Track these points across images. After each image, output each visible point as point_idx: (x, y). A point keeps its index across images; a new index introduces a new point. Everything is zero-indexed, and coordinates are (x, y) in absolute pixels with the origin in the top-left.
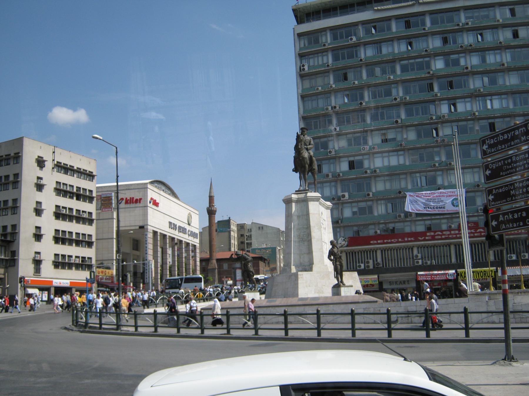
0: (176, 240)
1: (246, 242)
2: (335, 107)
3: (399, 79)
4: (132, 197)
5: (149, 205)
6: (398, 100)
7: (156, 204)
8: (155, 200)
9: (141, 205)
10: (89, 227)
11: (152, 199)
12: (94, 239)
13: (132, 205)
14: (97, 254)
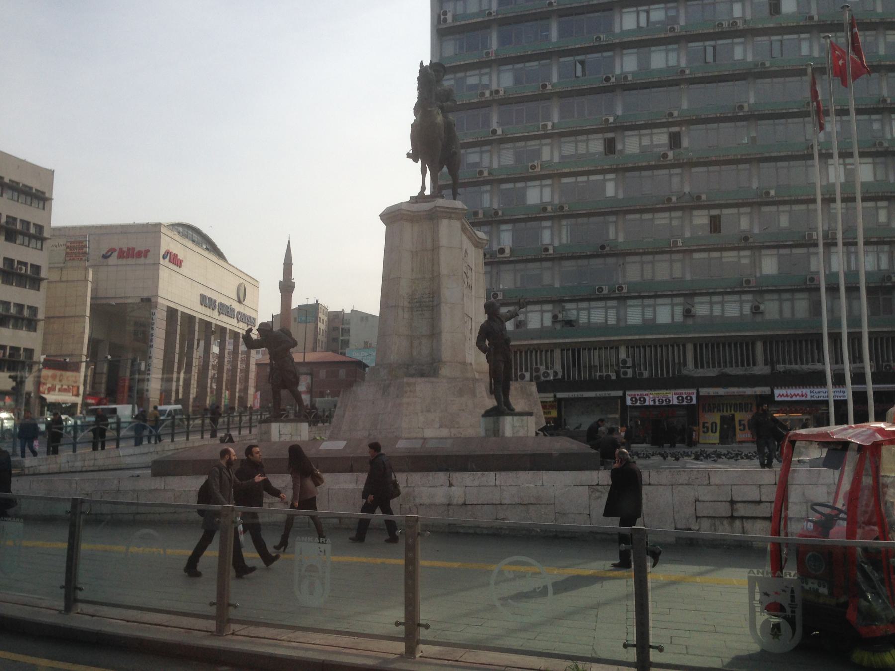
0: (213, 326)
1: (341, 338)
2: (497, 92)
3: (617, 41)
4: (131, 246)
5: (161, 261)
6: (613, 80)
7: (175, 261)
8: (175, 256)
9: (148, 261)
10: (32, 292)
11: (168, 253)
12: (41, 315)
13: (130, 261)
14: (45, 344)
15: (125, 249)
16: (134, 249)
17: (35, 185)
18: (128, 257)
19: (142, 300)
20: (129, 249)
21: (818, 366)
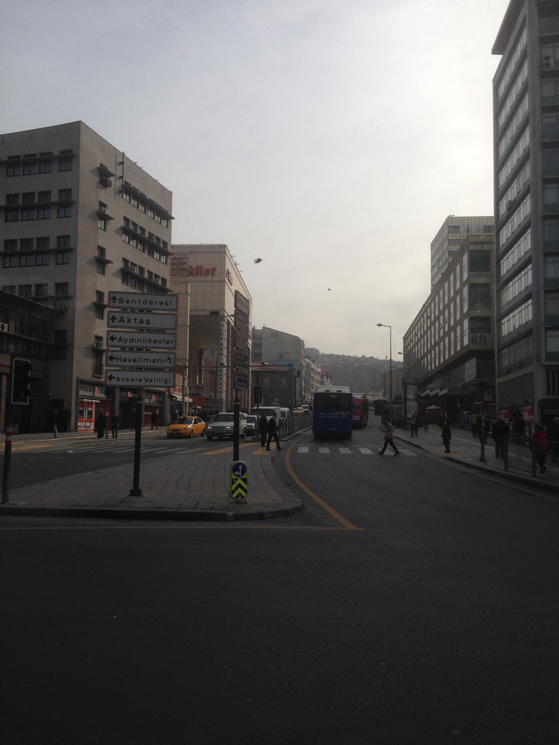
4: (199, 264)
13: (199, 278)
16: (202, 267)
17: (159, 201)
18: (196, 275)
19: (211, 312)
20: (197, 267)
21: (224, 410)
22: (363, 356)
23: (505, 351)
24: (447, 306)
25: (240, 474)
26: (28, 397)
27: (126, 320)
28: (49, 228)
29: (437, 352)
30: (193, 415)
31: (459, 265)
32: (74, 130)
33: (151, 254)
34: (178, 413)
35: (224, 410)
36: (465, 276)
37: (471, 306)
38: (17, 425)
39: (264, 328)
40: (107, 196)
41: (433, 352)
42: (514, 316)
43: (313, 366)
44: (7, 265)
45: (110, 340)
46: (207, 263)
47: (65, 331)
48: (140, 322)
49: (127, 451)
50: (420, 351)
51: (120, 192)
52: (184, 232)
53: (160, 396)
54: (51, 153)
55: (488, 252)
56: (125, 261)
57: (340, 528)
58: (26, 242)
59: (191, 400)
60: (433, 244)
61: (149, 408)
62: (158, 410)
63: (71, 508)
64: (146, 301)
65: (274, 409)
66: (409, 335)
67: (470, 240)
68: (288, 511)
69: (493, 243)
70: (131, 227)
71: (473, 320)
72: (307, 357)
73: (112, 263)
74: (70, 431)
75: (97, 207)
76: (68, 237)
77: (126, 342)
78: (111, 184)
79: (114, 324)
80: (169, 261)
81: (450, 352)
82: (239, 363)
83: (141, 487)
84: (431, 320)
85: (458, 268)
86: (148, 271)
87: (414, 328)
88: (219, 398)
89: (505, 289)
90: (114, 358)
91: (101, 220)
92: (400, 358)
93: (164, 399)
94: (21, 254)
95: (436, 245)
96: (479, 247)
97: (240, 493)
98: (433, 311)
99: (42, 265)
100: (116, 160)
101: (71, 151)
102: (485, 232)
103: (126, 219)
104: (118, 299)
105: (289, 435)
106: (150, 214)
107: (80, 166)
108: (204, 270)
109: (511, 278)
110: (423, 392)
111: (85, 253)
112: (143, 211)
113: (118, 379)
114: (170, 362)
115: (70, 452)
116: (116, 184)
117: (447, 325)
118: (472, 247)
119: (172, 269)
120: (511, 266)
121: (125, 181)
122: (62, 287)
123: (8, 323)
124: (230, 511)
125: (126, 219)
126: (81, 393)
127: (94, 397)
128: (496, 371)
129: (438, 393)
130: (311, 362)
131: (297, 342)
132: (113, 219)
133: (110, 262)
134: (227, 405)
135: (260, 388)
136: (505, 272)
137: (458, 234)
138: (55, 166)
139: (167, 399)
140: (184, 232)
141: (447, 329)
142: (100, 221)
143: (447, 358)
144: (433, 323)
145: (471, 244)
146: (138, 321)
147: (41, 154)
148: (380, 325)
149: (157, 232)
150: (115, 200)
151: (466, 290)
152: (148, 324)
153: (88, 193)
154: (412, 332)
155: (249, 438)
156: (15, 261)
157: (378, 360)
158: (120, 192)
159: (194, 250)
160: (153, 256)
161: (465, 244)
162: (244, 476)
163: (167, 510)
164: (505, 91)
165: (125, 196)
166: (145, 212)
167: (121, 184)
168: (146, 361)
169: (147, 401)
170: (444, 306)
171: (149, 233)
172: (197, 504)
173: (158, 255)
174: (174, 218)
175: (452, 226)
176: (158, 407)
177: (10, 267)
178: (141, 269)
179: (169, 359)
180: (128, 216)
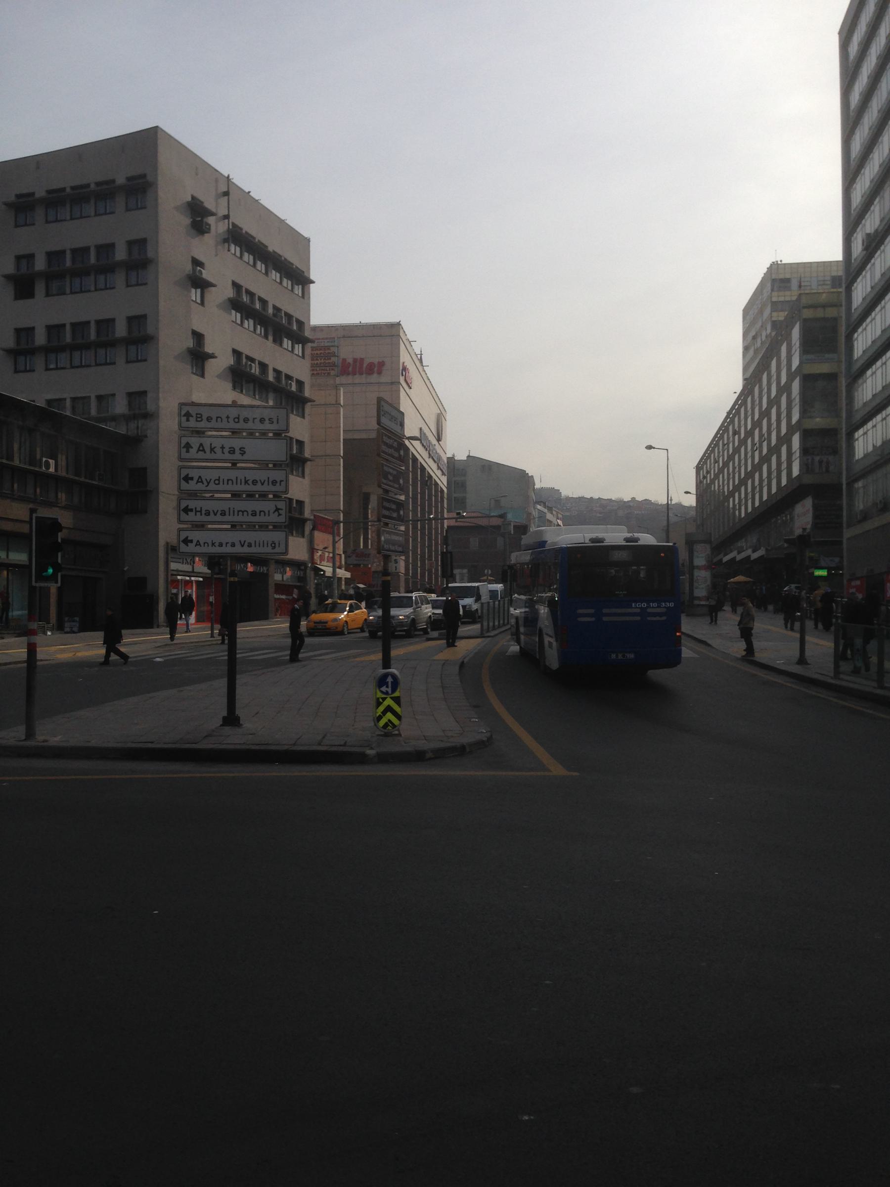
4: (358, 355)
13: (358, 379)
15: (350, 361)
16: (362, 360)
17: (289, 255)
18: (354, 374)
20: (355, 360)
21: (402, 589)
22: (633, 498)
23: (860, 484)
24: (766, 414)
25: (389, 690)
26: (59, 574)
27: (208, 449)
28: (111, 304)
29: (749, 489)
30: (350, 598)
31: (785, 345)
32: (147, 142)
33: (278, 341)
34: (326, 594)
35: (402, 589)
36: (796, 363)
37: (804, 412)
38: (77, 619)
39: (469, 456)
40: (203, 247)
41: (743, 489)
42: (874, 426)
43: (549, 516)
44: (52, 366)
45: (183, 482)
46: (370, 353)
47: (145, 469)
48: (229, 452)
49: (272, 655)
50: (723, 485)
51: (226, 241)
52: (333, 302)
53: (300, 569)
54: (113, 181)
55: (835, 320)
56: (237, 353)
57: (542, 773)
58: (80, 327)
59: (348, 575)
60: (746, 311)
61: (281, 588)
62: (296, 591)
63: (130, 745)
64: (238, 418)
65: (478, 587)
66: (706, 463)
67: (804, 301)
68: (463, 748)
69: (841, 306)
70: (245, 298)
71: (806, 435)
72: (539, 503)
73: (216, 357)
74: (158, 627)
75: (189, 267)
76: (144, 317)
77: (208, 483)
78: (209, 229)
79: (188, 456)
80: (308, 351)
81: (769, 489)
82: (386, 513)
83: (238, 712)
84: (739, 437)
85: (784, 348)
86: (275, 370)
87: (713, 451)
88: (394, 570)
89: (860, 381)
90: (191, 510)
91: (196, 288)
92: (690, 501)
93: (305, 574)
94: (74, 347)
95: (752, 313)
96: (820, 313)
97: (389, 720)
98: (743, 422)
99: (106, 364)
100: (216, 190)
101: (144, 176)
102: (833, 288)
103: (236, 286)
104: (195, 416)
105: (499, 627)
106: (275, 275)
107: (160, 201)
108: (365, 366)
109: (871, 362)
110: (726, 555)
111: (171, 342)
112: (263, 271)
113: (198, 544)
114: (279, 515)
115: (158, 659)
116: (218, 227)
117: (765, 444)
118: (808, 314)
119: (312, 366)
120: (869, 343)
121: (233, 224)
122: (137, 397)
123: (54, 457)
124: (372, 748)
125: (236, 286)
126: (173, 566)
127: (193, 572)
128: (845, 519)
129: (749, 557)
130: (546, 510)
131: (522, 478)
132: (214, 286)
133: (212, 356)
134: (407, 581)
135: (451, 553)
136: (860, 353)
137: (788, 293)
138: (120, 202)
139: (310, 574)
140: (333, 302)
141: (765, 451)
142: (193, 290)
143: (765, 498)
144: (743, 442)
145: (804, 307)
146: (226, 450)
147: (98, 184)
148: (650, 447)
149: (287, 306)
150: (216, 255)
151: (796, 386)
152: (242, 454)
153: (174, 246)
154: (709, 457)
155: (435, 634)
156: (64, 358)
157: (657, 505)
158: (226, 241)
159: (349, 332)
160: (281, 345)
161: (795, 309)
162: (397, 694)
163: (273, 748)
164: (858, 51)
165: (233, 247)
166: (266, 274)
167: (226, 228)
168: (241, 513)
169: (278, 577)
170: (761, 413)
171: (275, 307)
172: (324, 737)
173: (290, 342)
174: (313, 282)
175: (779, 278)
176: (296, 587)
177: (57, 368)
178: (263, 366)
179: (277, 510)
180: (238, 281)
